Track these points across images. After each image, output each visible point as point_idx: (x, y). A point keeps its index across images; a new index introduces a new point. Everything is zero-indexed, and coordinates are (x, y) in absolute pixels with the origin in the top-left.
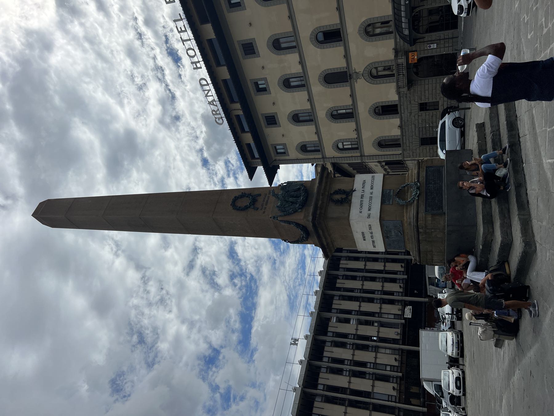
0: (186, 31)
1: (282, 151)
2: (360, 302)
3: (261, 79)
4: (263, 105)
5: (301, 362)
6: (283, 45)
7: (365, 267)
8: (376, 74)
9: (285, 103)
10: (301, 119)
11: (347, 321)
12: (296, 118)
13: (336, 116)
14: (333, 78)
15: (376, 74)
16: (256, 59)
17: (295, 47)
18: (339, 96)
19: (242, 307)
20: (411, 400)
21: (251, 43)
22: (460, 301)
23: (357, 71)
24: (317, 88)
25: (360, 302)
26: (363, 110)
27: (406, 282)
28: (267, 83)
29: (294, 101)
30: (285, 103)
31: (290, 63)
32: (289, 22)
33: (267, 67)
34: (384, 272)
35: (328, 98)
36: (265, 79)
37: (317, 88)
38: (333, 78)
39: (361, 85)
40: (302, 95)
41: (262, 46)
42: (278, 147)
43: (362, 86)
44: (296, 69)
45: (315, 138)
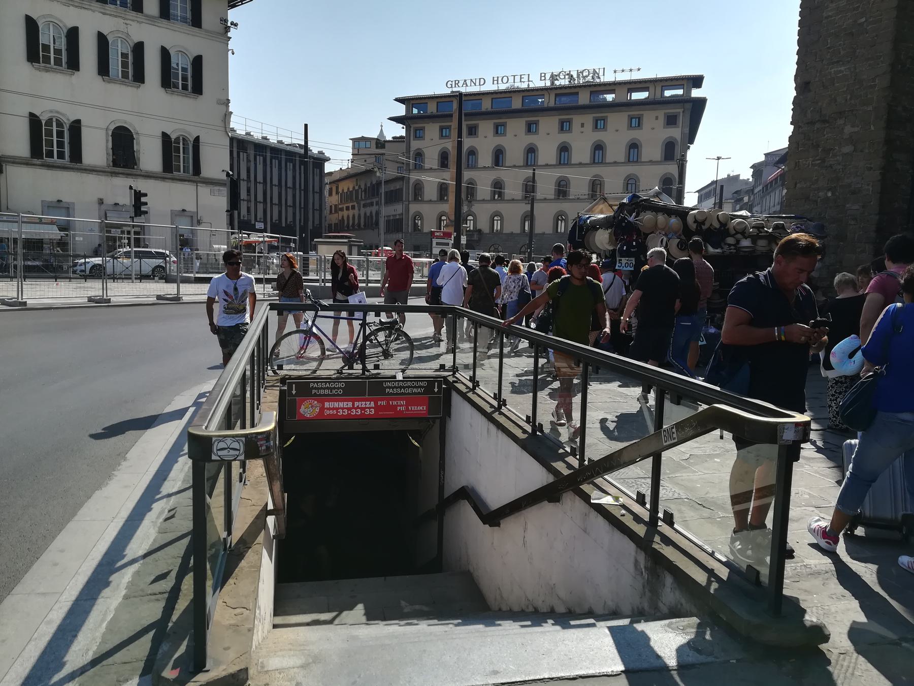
3: (505, 130)
6: (597, 152)
9: (581, 142)
10: (597, 152)
11: (472, 152)
12: (599, 147)
13: (498, 186)
14: (530, 188)
17: (629, 161)
18: (514, 189)
19: (643, 595)
20: (820, 646)
22: (741, 324)
24: (492, 175)
29: (581, 151)
30: (581, 142)
33: (515, 139)
37: (492, 175)
38: (530, 188)
40: (586, 158)
44: (609, 158)
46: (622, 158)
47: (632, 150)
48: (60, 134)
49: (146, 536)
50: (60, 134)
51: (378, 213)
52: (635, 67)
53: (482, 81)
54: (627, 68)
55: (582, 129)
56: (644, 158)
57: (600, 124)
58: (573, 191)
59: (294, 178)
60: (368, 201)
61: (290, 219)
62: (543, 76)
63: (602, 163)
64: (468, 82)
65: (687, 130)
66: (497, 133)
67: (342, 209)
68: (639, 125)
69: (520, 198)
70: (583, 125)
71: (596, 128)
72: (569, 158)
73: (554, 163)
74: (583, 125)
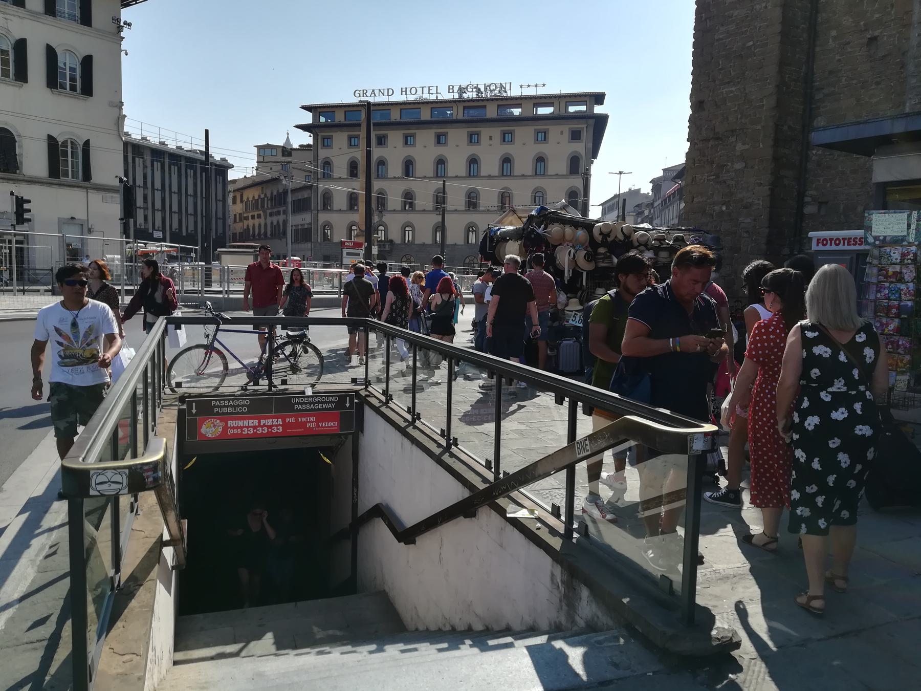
1: (353, 144)
14: (440, 200)
17: (470, 176)
40: (528, 169)
41: (507, 149)
58: (419, 203)
61: (191, 228)
63: (510, 175)
64: (377, 92)
67: (247, 218)
69: (345, 208)
74: (491, 138)
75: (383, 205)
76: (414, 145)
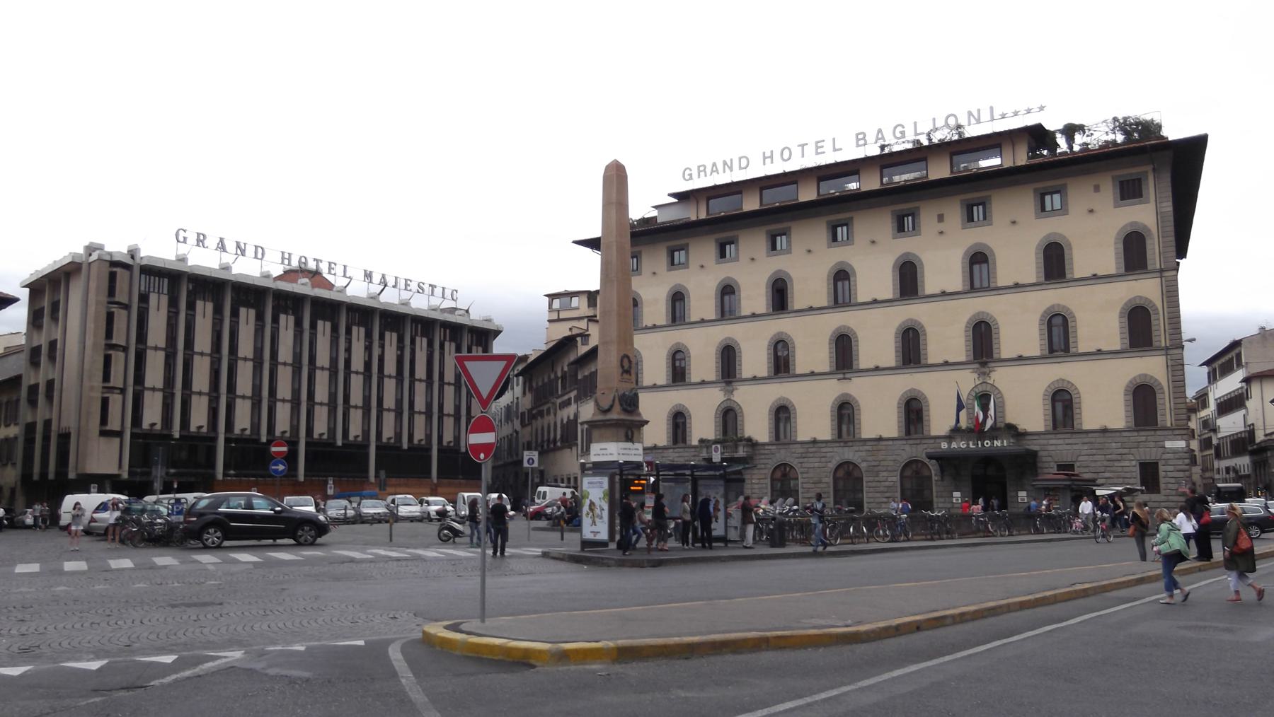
0: (817, 153)
2: (164, 349)
3: (789, 242)
4: (752, 244)
5: (182, 259)
6: (840, 284)
7: (161, 349)
8: (729, 416)
10: (726, 298)
14: (728, 357)
15: (729, 416)
16: (959, 221)
18: (703, 365)
21: (1141, 196)
23: (992, 374)
25: (164, 349)
26: (679, 397)
27: (330, 444)
28: (783, 252)
31: (754, 297)
32: (937, 291)
34: (141, 346)
35: (702, 347)
36: (789, 251)
39: (832, 389)
40: (821, 296)
41: (838, 255)
42: (683, 253)
43: (716, 397)
44: (1004, 277)
45: (694, 317)
46: (823, 299)
47: (976, 267)
48: (46, 438)
49: (89, 342)
50: (46, 438)
51: (576, 416)
52: (1035, 106)
53: (745, 162)
54: (1035, 106)
55: (941, 226)
56: (1003, 278)
57: (978, 212)
58: (934, 350)
59: (348, 350)
60: (566, 397)
61: (419, 435)
62: (861, 138)
65: (1168, 207)
66: (673, 263)
68: (985, 218)
69: (826, 368)
70: (941, 218)
71: (673, 263)
72: (991, 274)
73: (959, 288)
74: (941, 218)
75: (989, 353)
76: (789, 251)
